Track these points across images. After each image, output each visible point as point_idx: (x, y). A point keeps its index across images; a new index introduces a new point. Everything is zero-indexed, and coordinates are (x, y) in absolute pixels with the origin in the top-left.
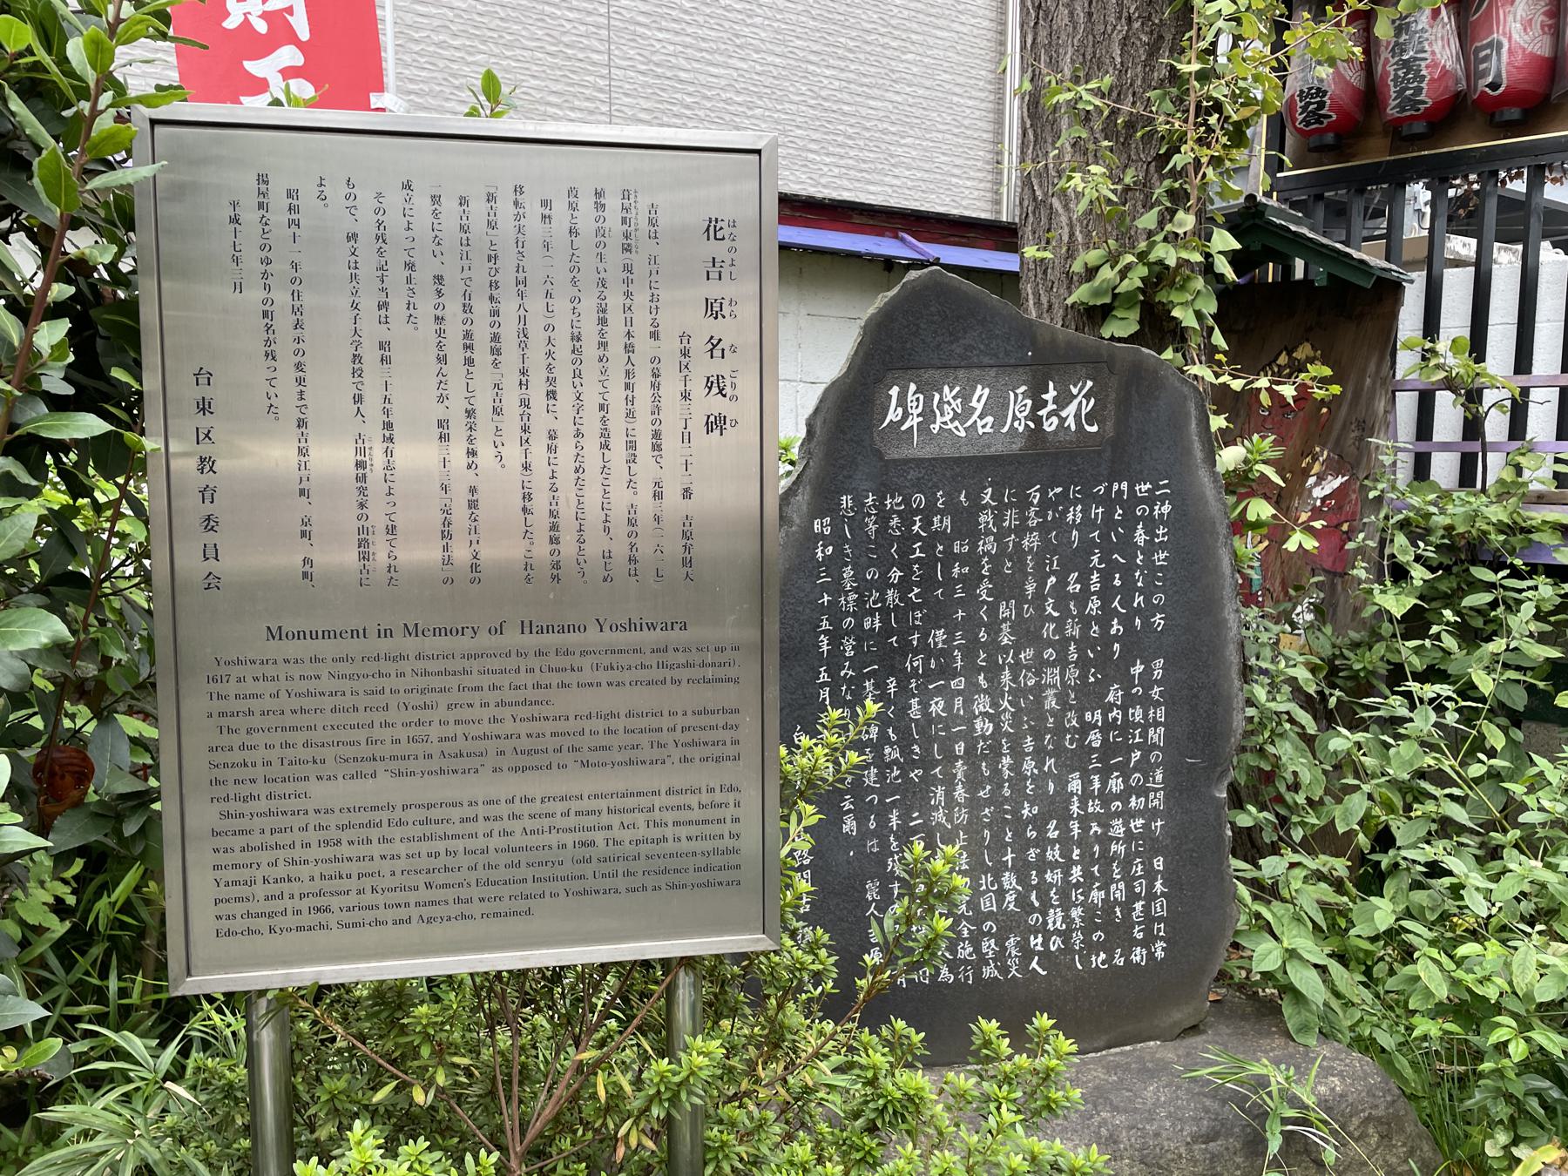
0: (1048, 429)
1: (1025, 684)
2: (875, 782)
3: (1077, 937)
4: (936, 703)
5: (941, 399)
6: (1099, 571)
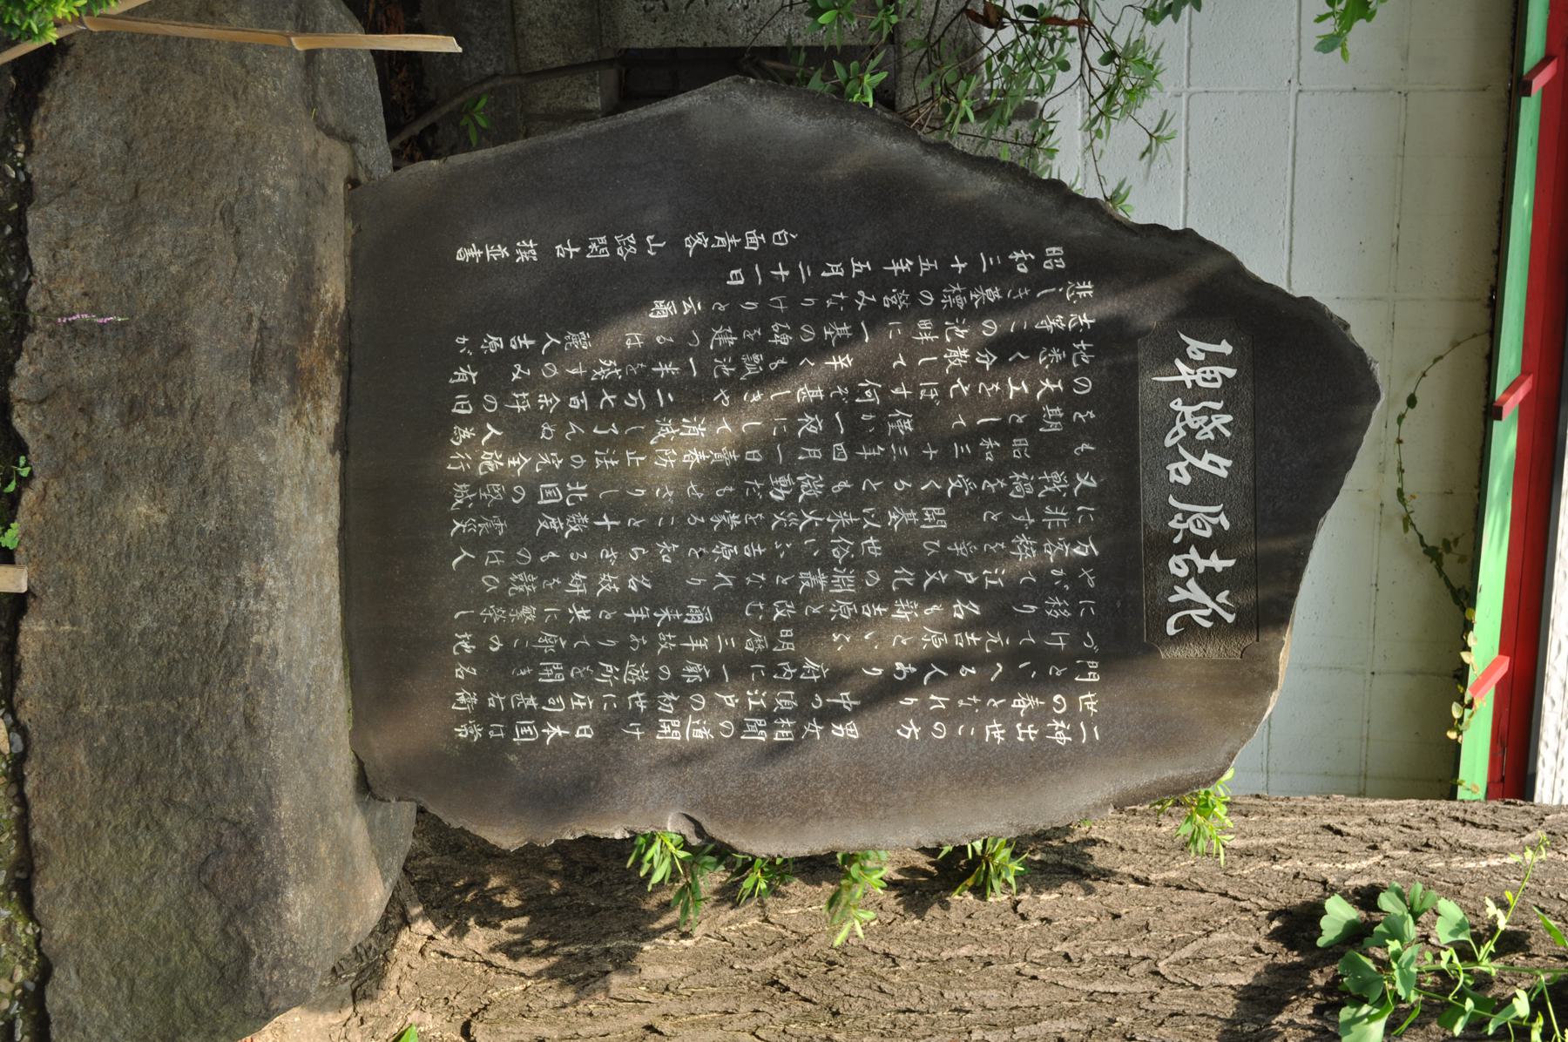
0: (1171, 564)
1: (834, 545)
2: (716, 342)
3: (495, 613)
4: (815, 424)
5: (1215, 412)
6: (981, 645)
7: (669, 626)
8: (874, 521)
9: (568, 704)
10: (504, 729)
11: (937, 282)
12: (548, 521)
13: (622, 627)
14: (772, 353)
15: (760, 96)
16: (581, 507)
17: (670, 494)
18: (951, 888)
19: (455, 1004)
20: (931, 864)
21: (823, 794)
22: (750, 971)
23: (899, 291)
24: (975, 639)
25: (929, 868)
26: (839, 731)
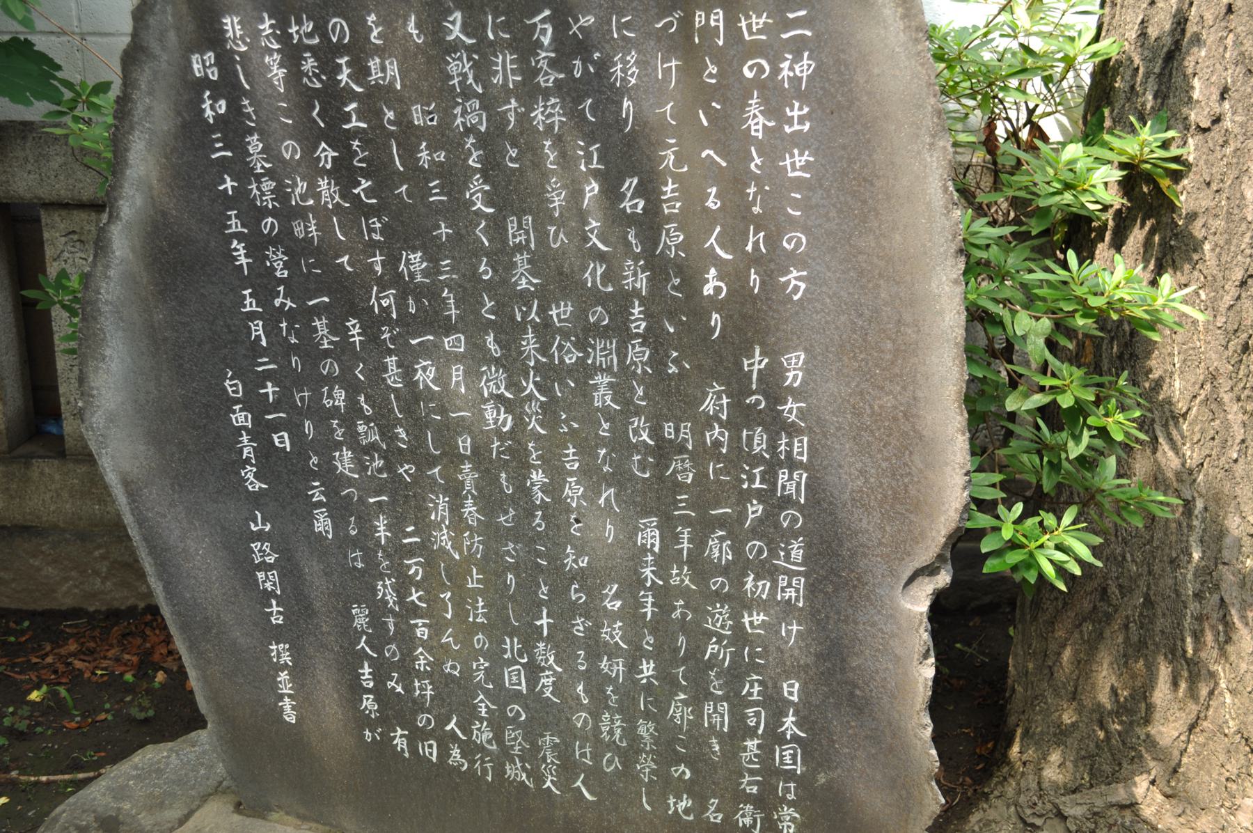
3: (646, 766)
4: (424, 369)
6: (677, 178)
7: (662, 567)
8: (530, 308)
9: (756, 703)
10: (786, 782)
11: (253, 214)
12: (544, 686)
13: (660, 625)
14: (354, 411)
15: (93, 396)
16: (528, 647)
17: (511, 546)
18: (1172, 207)
19: (1235, 771)
20: (1142, 226)
21: (881, 407)
22: (1243, 441)
23: (267, 257)
24: (670, 187)
25: (1147, 228)
26: (795, 377)
